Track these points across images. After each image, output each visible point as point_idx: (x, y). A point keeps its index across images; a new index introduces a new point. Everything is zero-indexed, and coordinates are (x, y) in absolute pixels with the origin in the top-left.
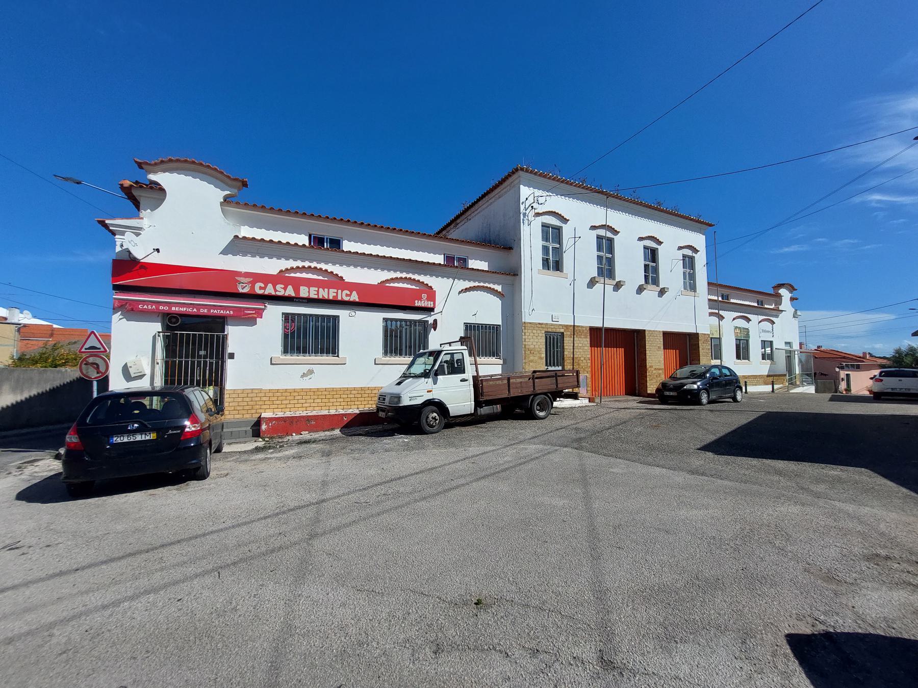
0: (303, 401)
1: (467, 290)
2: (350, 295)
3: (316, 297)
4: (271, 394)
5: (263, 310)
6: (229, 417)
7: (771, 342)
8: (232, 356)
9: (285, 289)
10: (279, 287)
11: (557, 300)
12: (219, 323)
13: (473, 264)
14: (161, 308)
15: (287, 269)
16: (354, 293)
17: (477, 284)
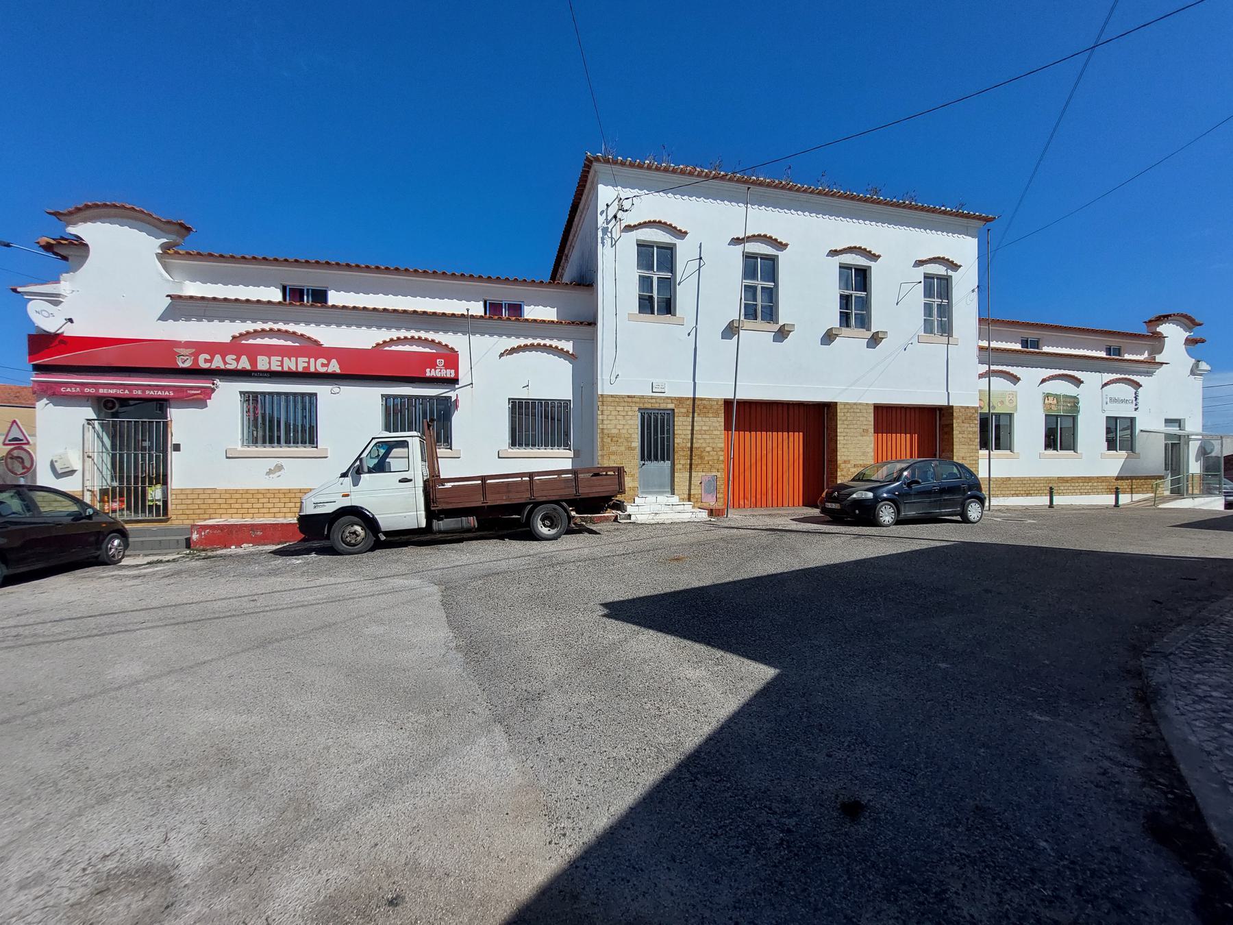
0: (270, 505)
1: (513, 351)
2: (327, 365)
3: (280, 369)
4: (228, 496)
5: (213, 390)
6: (176, 522)
7: (1132, 420)
8: (177, 448)
9: (238, 360)
10: (229, 358)
11: (640, 360)
12: (161, 405)
13: (530, 312)
14: (87, 390)
15: (241, 335)
16: (334, 362)
17: (529, 341)
